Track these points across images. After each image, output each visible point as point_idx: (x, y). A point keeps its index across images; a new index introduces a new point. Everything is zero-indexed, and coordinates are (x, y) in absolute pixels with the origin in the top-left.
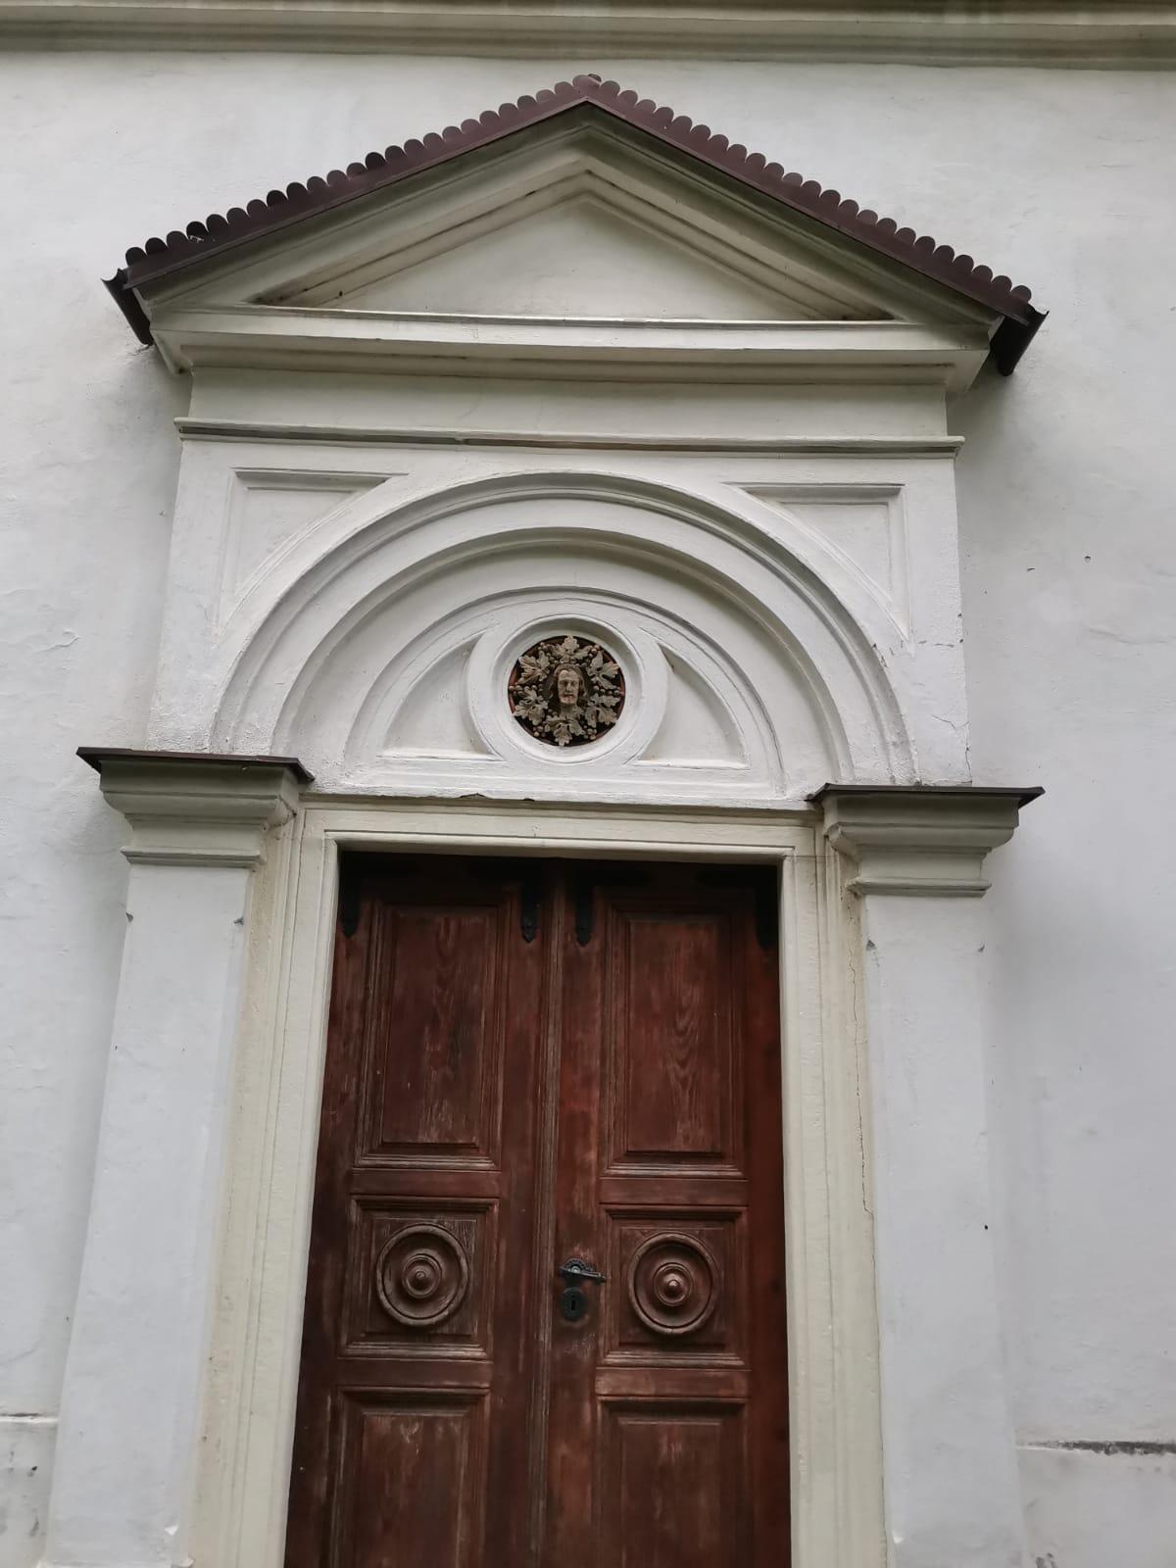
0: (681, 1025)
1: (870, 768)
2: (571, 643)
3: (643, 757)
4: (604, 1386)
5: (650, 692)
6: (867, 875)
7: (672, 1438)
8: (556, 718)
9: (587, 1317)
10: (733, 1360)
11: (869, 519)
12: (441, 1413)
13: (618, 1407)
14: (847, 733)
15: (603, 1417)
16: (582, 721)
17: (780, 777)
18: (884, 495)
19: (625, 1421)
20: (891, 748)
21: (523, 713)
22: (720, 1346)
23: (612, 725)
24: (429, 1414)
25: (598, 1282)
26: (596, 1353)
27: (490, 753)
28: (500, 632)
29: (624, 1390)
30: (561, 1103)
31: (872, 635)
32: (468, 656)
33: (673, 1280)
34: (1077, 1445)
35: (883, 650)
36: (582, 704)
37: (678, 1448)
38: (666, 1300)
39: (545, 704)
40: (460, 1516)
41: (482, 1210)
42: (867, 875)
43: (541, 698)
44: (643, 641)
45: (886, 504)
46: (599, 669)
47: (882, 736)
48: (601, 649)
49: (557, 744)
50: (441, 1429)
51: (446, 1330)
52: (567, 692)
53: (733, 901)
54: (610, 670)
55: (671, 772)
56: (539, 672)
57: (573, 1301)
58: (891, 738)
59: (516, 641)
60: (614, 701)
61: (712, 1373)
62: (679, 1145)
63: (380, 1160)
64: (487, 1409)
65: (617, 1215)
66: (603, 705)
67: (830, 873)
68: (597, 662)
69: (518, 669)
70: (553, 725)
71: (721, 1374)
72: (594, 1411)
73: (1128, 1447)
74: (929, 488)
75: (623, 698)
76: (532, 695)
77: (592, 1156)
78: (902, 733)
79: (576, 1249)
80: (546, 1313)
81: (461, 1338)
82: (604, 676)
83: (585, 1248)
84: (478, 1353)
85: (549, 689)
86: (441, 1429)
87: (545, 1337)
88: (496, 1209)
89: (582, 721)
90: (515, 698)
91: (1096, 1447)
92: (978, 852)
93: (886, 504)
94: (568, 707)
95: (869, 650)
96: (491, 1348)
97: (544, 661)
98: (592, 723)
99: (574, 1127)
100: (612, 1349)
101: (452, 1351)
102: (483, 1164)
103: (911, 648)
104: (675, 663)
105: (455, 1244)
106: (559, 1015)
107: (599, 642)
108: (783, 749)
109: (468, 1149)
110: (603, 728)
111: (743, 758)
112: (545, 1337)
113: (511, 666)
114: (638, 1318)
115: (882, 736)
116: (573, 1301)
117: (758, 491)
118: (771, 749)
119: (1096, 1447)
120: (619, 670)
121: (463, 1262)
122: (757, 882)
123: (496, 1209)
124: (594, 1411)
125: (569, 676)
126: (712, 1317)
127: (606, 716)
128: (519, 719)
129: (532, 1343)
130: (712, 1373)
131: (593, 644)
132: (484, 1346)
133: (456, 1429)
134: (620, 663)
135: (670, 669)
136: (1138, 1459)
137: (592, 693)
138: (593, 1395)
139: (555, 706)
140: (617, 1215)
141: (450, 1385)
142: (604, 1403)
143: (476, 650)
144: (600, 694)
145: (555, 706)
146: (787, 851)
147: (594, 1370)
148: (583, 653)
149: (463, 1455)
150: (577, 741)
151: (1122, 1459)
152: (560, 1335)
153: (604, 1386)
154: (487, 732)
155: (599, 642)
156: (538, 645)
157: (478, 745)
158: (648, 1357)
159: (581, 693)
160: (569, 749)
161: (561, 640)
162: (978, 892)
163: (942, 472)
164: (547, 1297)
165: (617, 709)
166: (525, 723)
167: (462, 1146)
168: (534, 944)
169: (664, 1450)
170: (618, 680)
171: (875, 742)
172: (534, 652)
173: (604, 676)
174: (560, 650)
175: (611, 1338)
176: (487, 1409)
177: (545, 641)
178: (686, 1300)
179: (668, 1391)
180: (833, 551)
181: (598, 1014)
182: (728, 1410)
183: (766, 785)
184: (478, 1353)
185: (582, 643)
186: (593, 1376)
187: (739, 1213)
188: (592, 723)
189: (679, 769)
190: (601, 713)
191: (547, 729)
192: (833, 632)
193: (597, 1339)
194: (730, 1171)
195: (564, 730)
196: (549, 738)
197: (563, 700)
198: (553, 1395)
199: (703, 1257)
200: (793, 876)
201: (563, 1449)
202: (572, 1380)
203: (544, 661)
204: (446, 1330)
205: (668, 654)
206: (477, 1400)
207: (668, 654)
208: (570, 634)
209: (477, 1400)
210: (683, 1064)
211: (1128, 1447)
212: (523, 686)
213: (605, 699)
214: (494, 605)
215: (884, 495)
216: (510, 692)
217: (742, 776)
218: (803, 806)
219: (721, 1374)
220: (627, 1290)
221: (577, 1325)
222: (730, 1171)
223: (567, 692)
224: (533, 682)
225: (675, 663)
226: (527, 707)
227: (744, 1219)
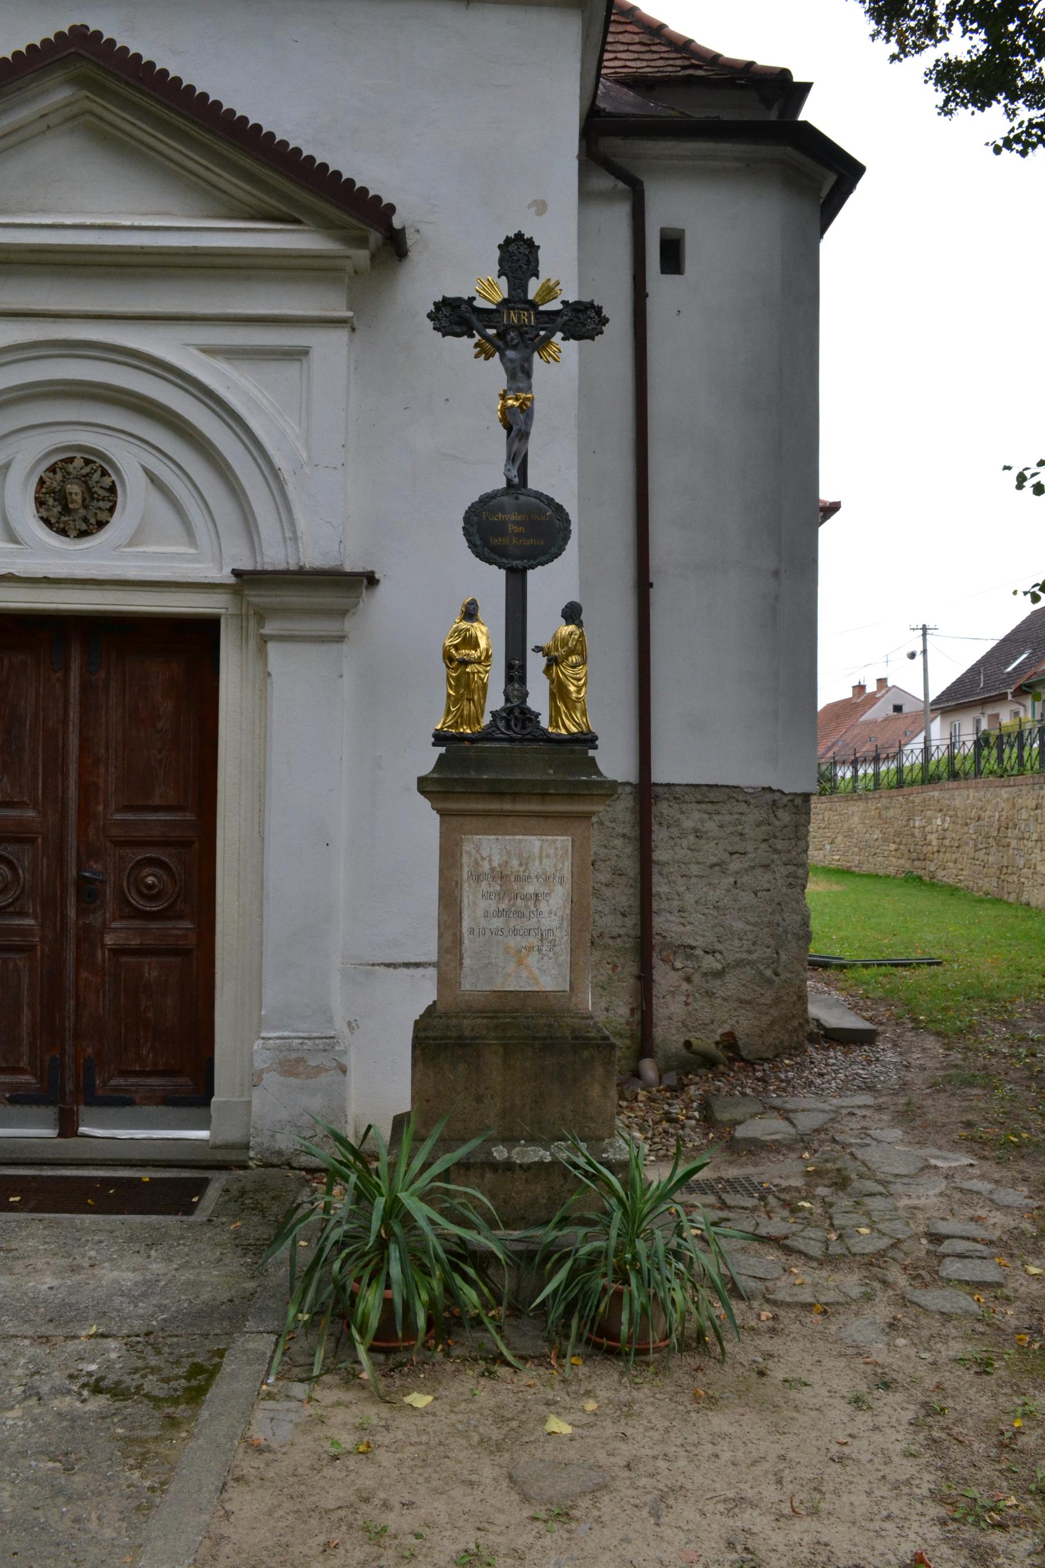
0: (159, 725)
1: (275, 556)
2: (78, 463)
3: (130, 545)
4: (109, 940)
5: (135, 498)
6: (268, 629)
7: (151, 970)
8: (67, 518)
9: (98, 902)
10: (188, 925)
11: (290, 370)
12: (11, 955)
13: (118, 952)
14: (261, 530)
15: (109, 958)
16: (85, 520)
17: (219, 558)
18: (298, 354)
19: (123, 959)
20: (288, 541)
21: (45, 514)
22: (180, 917)
23: (107, 522)
24: (6, 956)
25: (102, 882)
26: (104, 923)
27: (20, 544)
28: (28, 457)
29: (121, 942)
30: (80, 775)
31: (278, 461)
32: (6, 473)
33: (150, 880)
34: (378, 965)
35: (286, 474)
36: (86, 507)
37: (154, 974)
38: (145, 891)
39: (59, 509)
40: (25, 1010)
41: (32, 841)
42: (268, 629)
43: (56, 503)
44: (128, 461)
45: (301, 360)
46: (97, 482)
47: (283, 533)
48: (101, 466)
49: (68, 536)
50: (11, 965)
51: (12, 909)
52: (77, 497)
53: (191, 644)
54: (106, 482)
55: (145, 556)
56: (55, 484)
57: (88, 893)
58: (288, 534)
59: (39, 461)
60: (108, 505)
61: (175, 932)
62: (157, 801)
63: (130, 817)
64: (39, 953)
65: (117, 844)
66: (100, 509)
67: (251, 624)
68: (96, 476)
69: (42, 482)
70: (65, 523)
71: (180, 932)
72: (103, 954)
73: (407, 965)
74: (330, 348)
75: (115, 503)
76: (51, 502)
77: (101, 808)
78: (294, 532)
79: (91, 863)
80: (72, 900)
81: (22, 914)
82: (101, 487)
83: (96, 862)
84: (32, 922)
85: (62, 498)
86: (11, 965)
87: (72, 913)
88: (40, 840)
89: (85, 520)
90: (40, 503)
91: (388, 965)
92: (342, 613)
93: (301, 360)
94: (76, 510)
95: (275, 472)
96: (40, 920)
97: (59, 476)
98: (93, 521)
99: (88, 791)
100: (114, 920)
101: (17, 922)
102: (31, 814)
103: (307, 469)
104: (153, 479)
105: (15, 861)
106: (77, 721)
107: (99, 461)
108: (222, 541)
109: (20, 805)
110: (101, 525)
111: (197, 548)
112: (72, 913)
113: (35, 480)
114: (129, 902)
115: (283, 533)
116: (88, 893)
117: (209, 351)
118: (215, 540)
119: (388, 965)
120: (113, 482)
121: (20, 871)
122: (191, 644)
123: (40, 840)
124: (103, 954)
125: (74, 489)
126: (175, 901)
127: (102, 516)
128: (42, 518)
129: (64, 917)
130: (175, 932)
131: (95, 462)
132: (35, 917)
133: (21, 964)
134: (114, 477)
135: (148, 481)
136: (412, 971)
137: (93, 499)
138: (103, 945)
139: (66, 510)
140: (117, 844)
141: (16, 940)
142: (110, 950)
143: (12, 469)
144: (98, 500)
145: (66, 510)
146: (222, 611)
147: (105, 929)
148: (87, 470)
149: (26, 979)
150: (83, 534)
151: (404, 971)
152: (81, 912)
153: (109, 940)
154: (20, 530)
155: (99, 461)
156: (56, 463)
157: (13, 539)
158: (136, 923)
159: (84, 500)
160: (77, 540)
161: (71, 460)
162: (340, 639)
163: (339, 337)
164: (72, 891)
165: (111, 510)
166: (46, 521)
167: (19, 803)
168: (60, 674)
169: (146, 974)
170: (112, 489)
171: (279, 535)
172: (52, 469)
173: (101, 487)
174: (70, 468)
175: (114, 913)
176: (39, 953)
177: (61, 461)
178: (159, 892)
179: (148, 942)
180: (260, 396)
181: (104, 719)
182: (183, 952)
183: (211, 565)
184: (32, 922)
185: (87, 462)
186: (102, 934)
187: (193, 842)
188: (93, 521)
189: (151, 555)
190: (99, 514)
191: (62, 526)
192: (254, 459)
193: (105, 913)
194: (189, 817)
195: (72, 526)
196: (63, 532)
197: (71, 506)
198: (78, 947)
199: (168, 866)
200: (227, 626)
201: (84, 974)
202: (88, 937)
203: (59, 476)
204: (12, 909)
205: (147, 471)
206: (32, 948)
207: (147, 471)
208: (78, 455)
209: (32, 948)
210: (160, 751)
211: (407, 965)
212: (45, 494)
213: (101, 504)
214: (23, 435)
215: (298, 354)
216: (36, 499)
217: (194, 559)
218: (232, 580)
219: (180, 932)
220: (122, 886)
221: (93, 906)
222: (189, 817)
223: (77, 497)
224: (51, 492)
225: (153, 479)
226: (47, 510)
227: (196, 845)
